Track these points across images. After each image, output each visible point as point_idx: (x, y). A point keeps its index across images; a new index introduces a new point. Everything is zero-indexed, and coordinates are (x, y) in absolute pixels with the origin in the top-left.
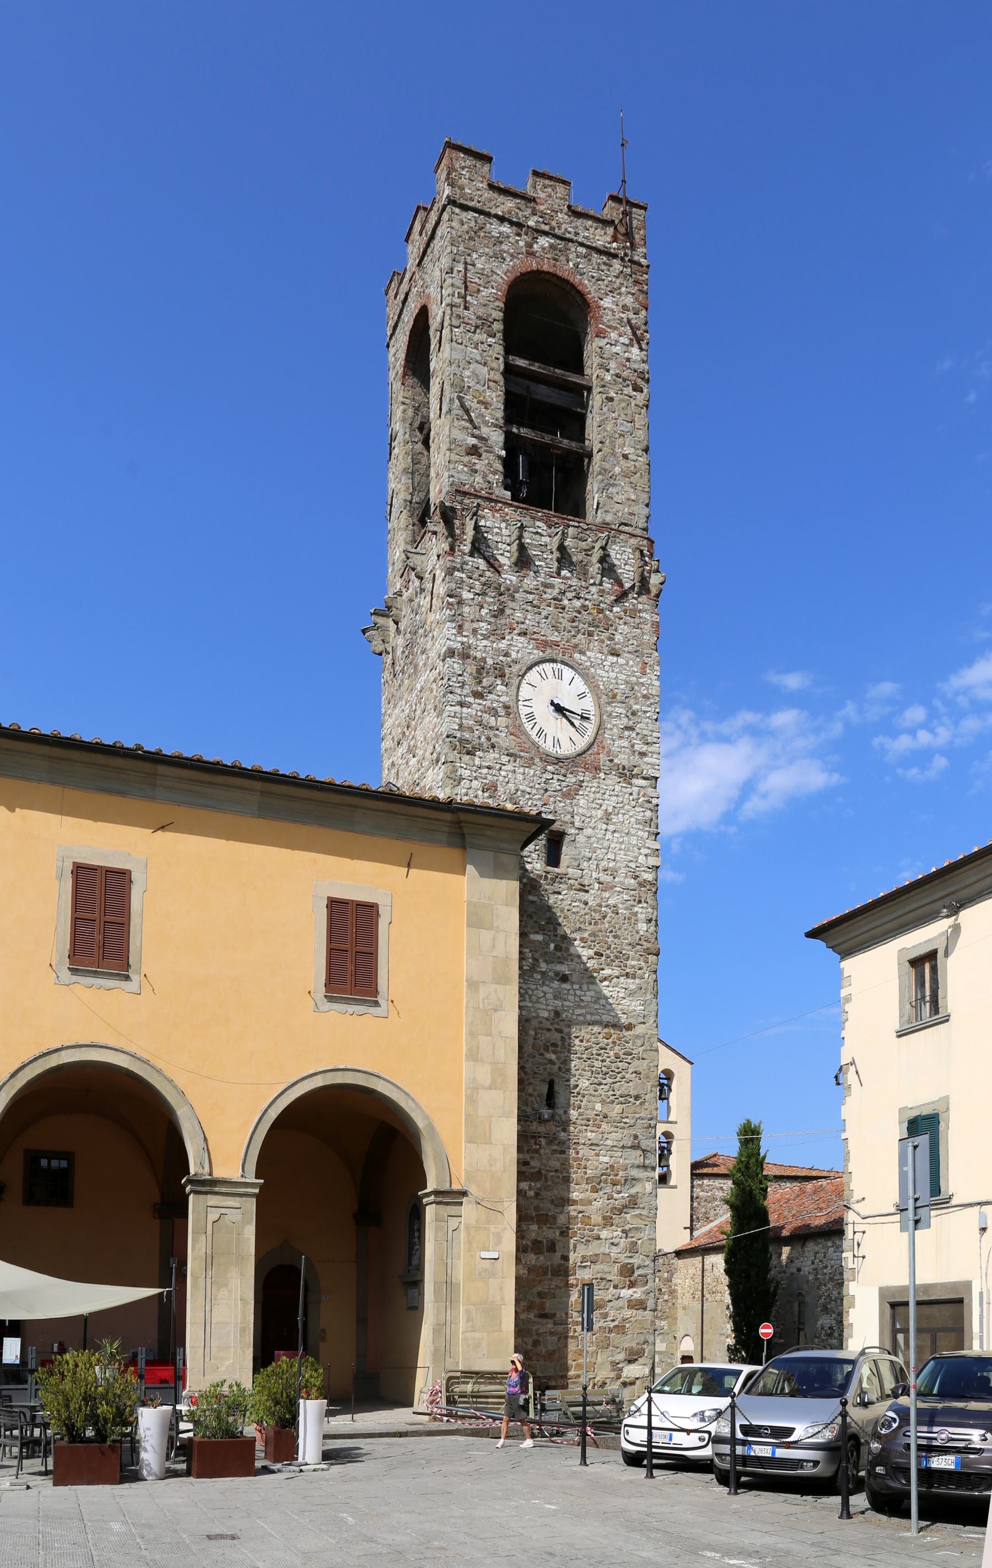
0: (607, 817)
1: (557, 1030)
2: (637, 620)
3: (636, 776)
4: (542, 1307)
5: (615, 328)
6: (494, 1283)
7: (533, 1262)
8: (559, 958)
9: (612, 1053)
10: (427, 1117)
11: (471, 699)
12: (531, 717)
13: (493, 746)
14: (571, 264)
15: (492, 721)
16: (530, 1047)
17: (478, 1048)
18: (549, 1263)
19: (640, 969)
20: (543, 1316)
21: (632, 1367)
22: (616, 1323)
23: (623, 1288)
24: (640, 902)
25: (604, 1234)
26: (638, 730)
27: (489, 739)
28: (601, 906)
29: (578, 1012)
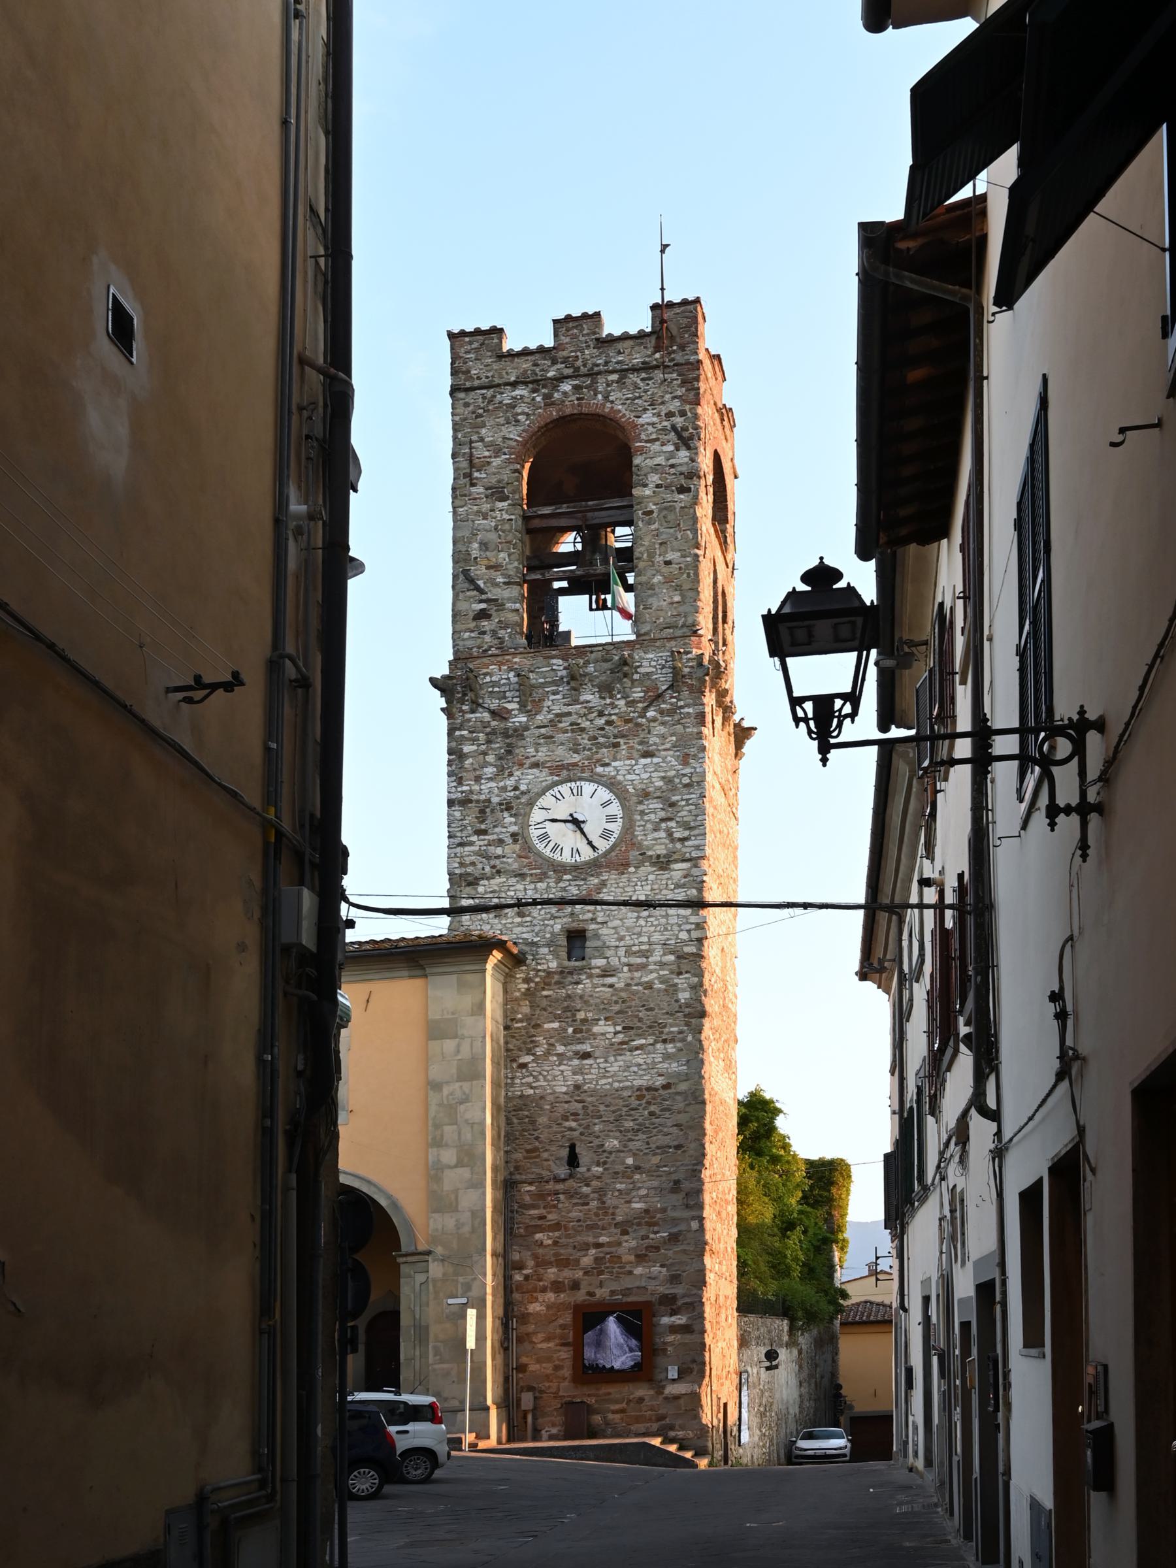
2: (677, 717)
10: (389, 1197)
11: (474, 838)
13: (499, 872)
14: (600, 397)
15: (499, 851)
24: (680, 973)
27: (493, 867)
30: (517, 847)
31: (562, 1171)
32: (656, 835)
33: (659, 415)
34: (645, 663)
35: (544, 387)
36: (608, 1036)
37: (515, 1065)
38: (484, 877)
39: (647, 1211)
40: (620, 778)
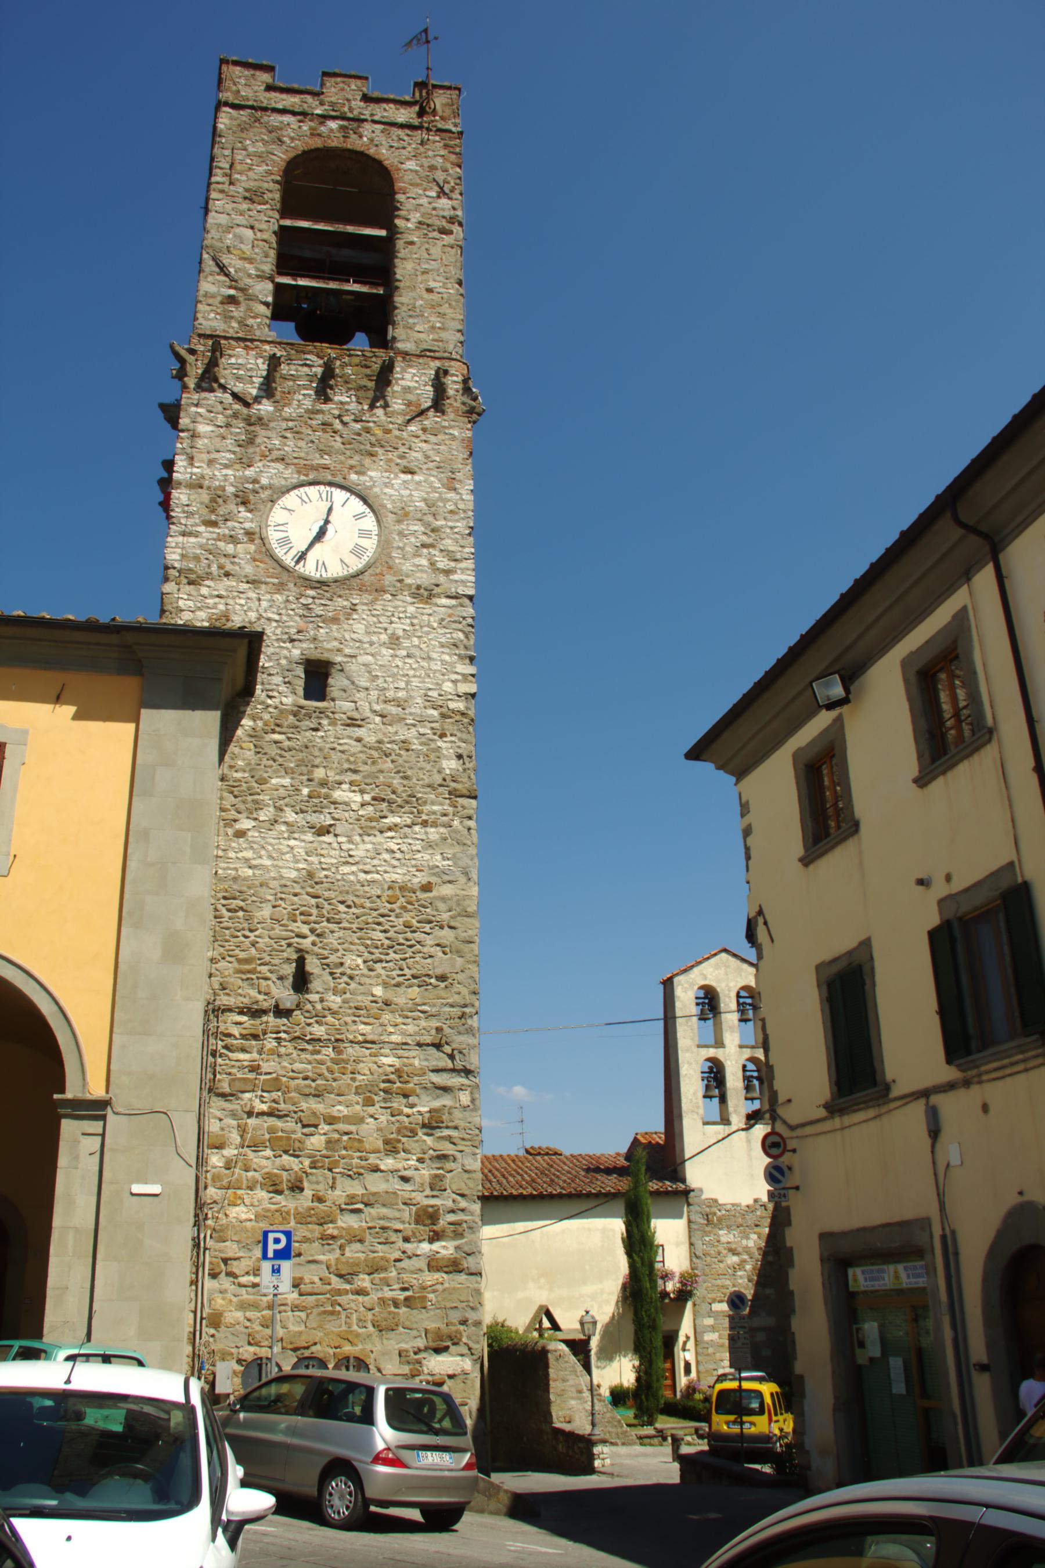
3: (439, 596)
5: (418, 185)
13: (227, 575)
14: (365, 139)
15: (230, 548)
19: (445, 815)
21: (441, 1358)
29: (346, 869)
30: (252, 548)
31: (285, 995)
32: (417, 561)
33: (422, 166)
34: (408, 376)
35: (311, 121)
36: (354, 807)
37: (230, 831)
38: (209, 576)
39: (398, 1072)
40: (376, 490)
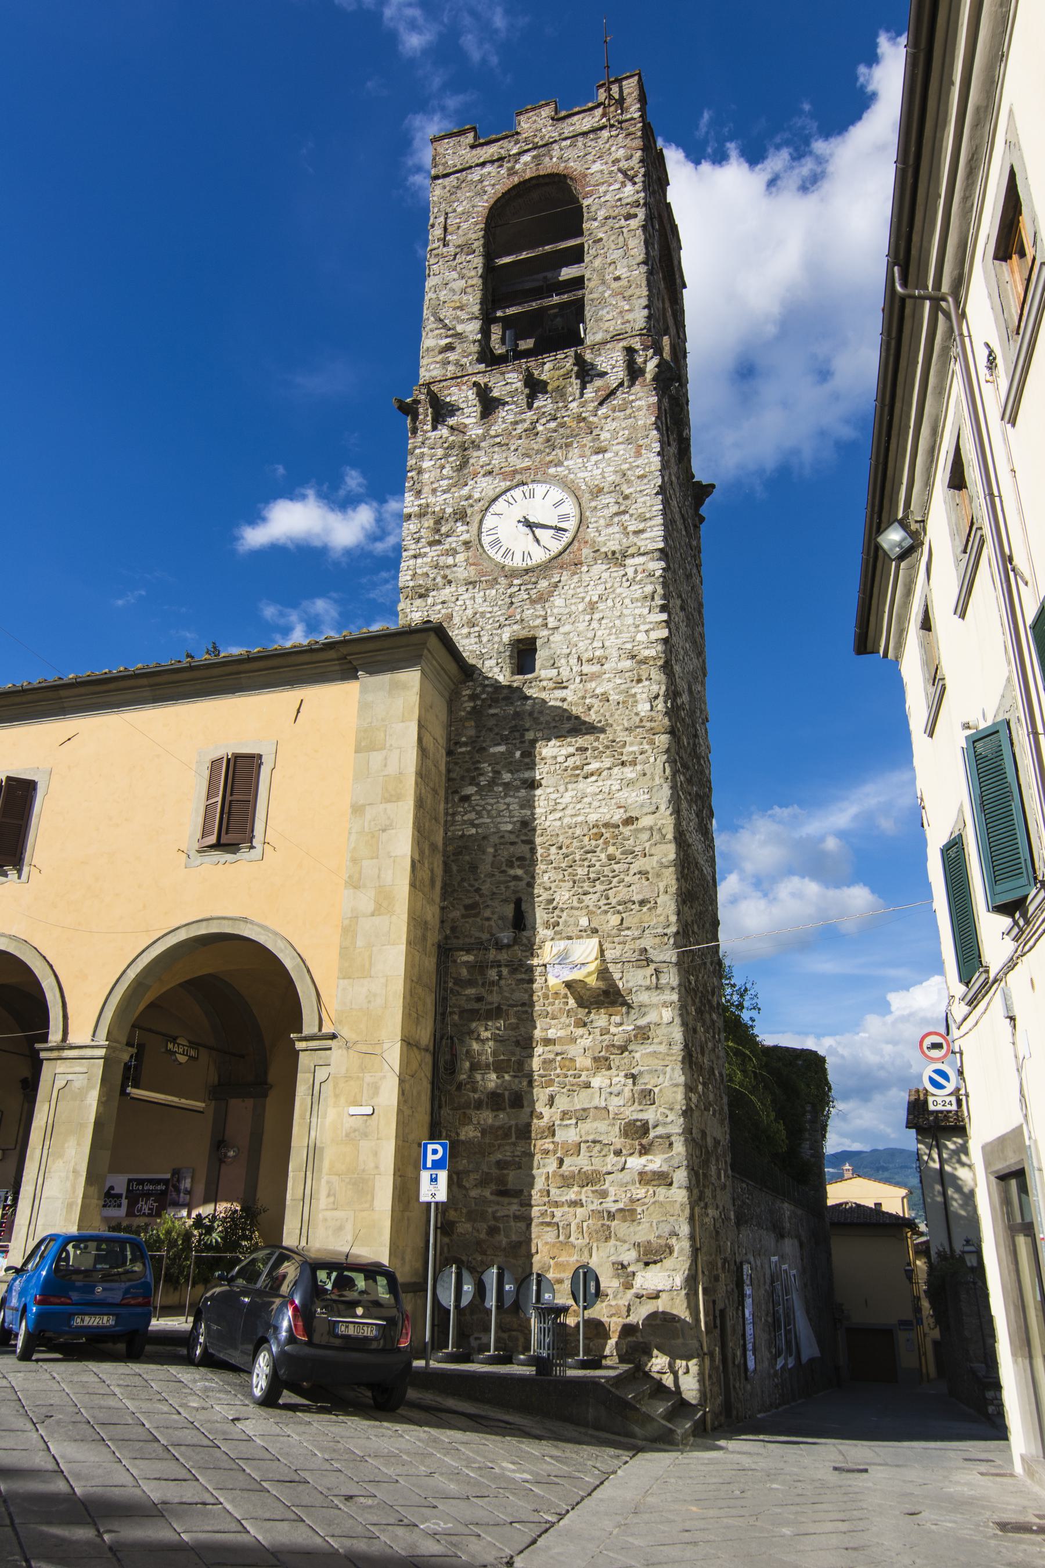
0: (592, 607)
1: (523, 842)
4: (502, 1180)
6: (365, 1145)
7: (490, 1121)
8: (527, 764)
9: (603, 856)
12: (497, 542)
15: (450, 561)
16: (488, 867)
17: (360, 873)
18: (513, 1122)
20: (504, 1193)
22: (621, 1205)
23: (631, 1154)
24: (639, 681)
25: (596, 1082)
26: (631, 512)
27: (445, 577)
28: (584, 698)
